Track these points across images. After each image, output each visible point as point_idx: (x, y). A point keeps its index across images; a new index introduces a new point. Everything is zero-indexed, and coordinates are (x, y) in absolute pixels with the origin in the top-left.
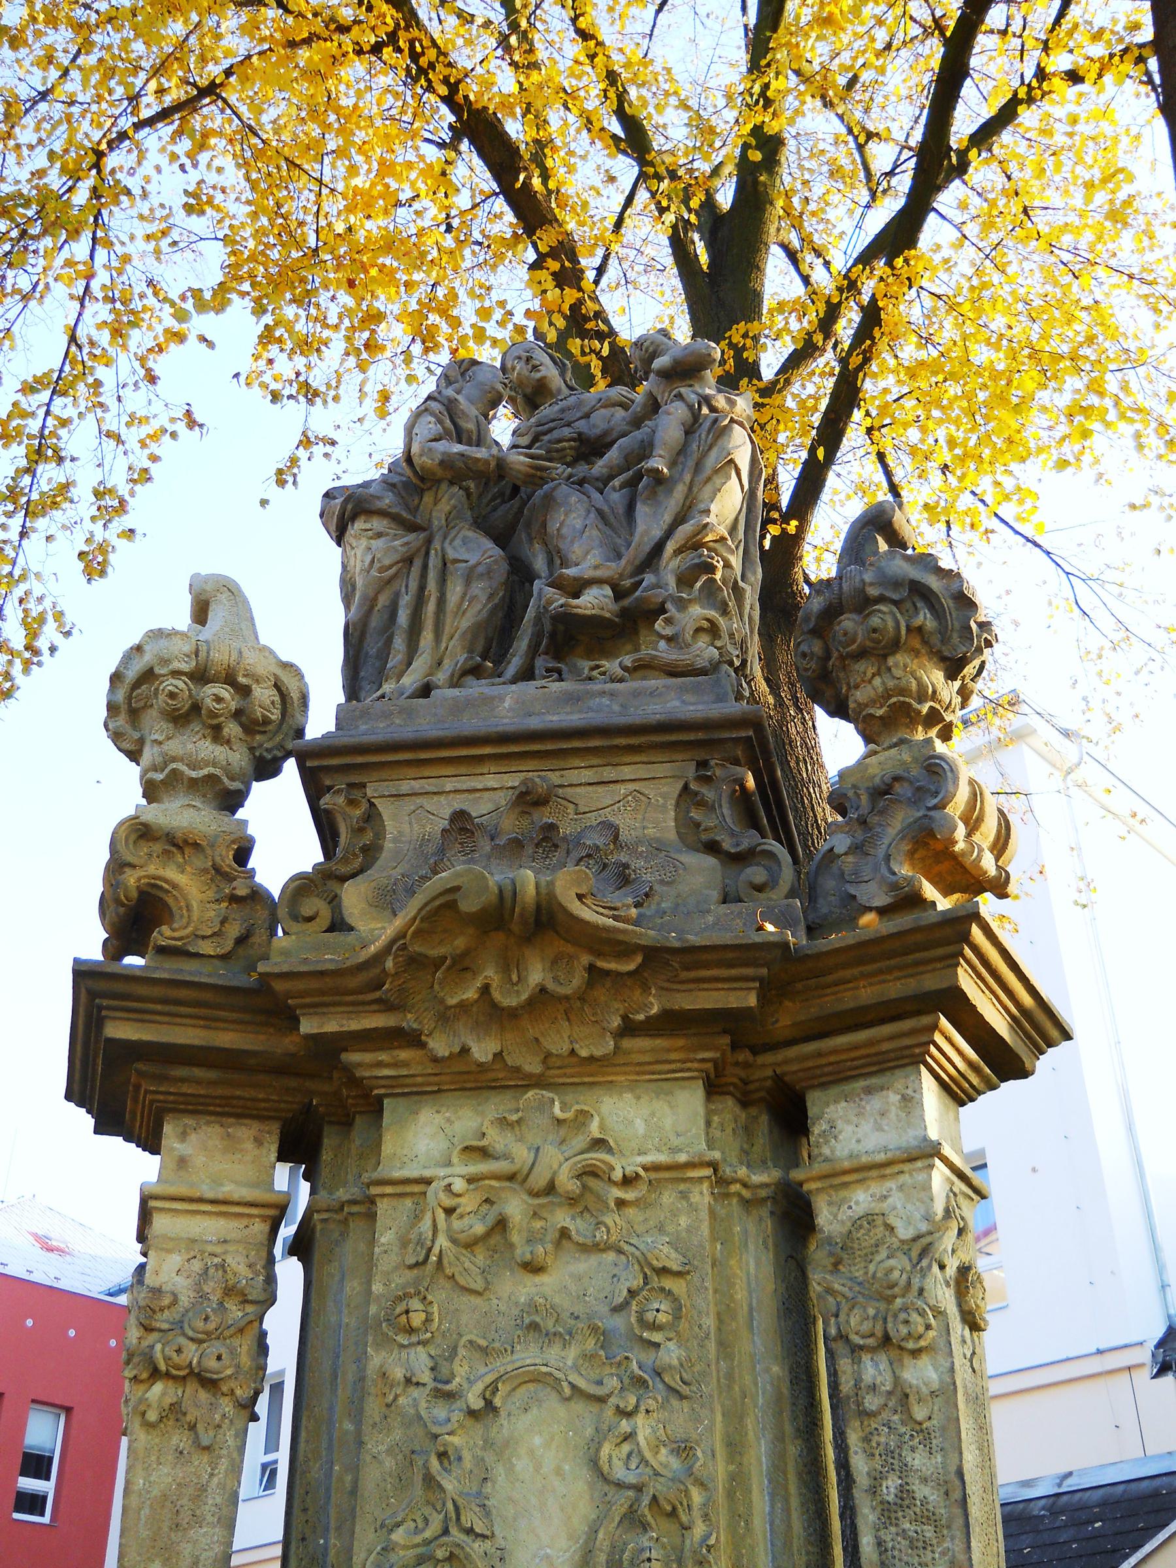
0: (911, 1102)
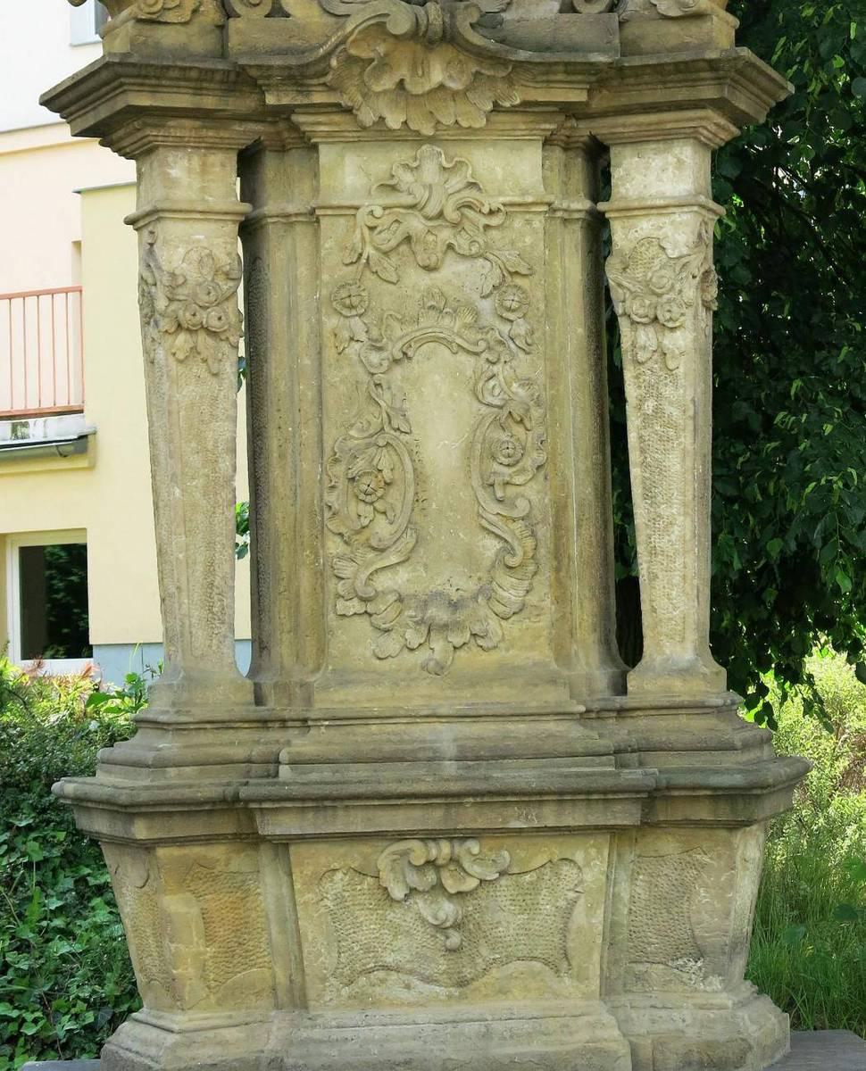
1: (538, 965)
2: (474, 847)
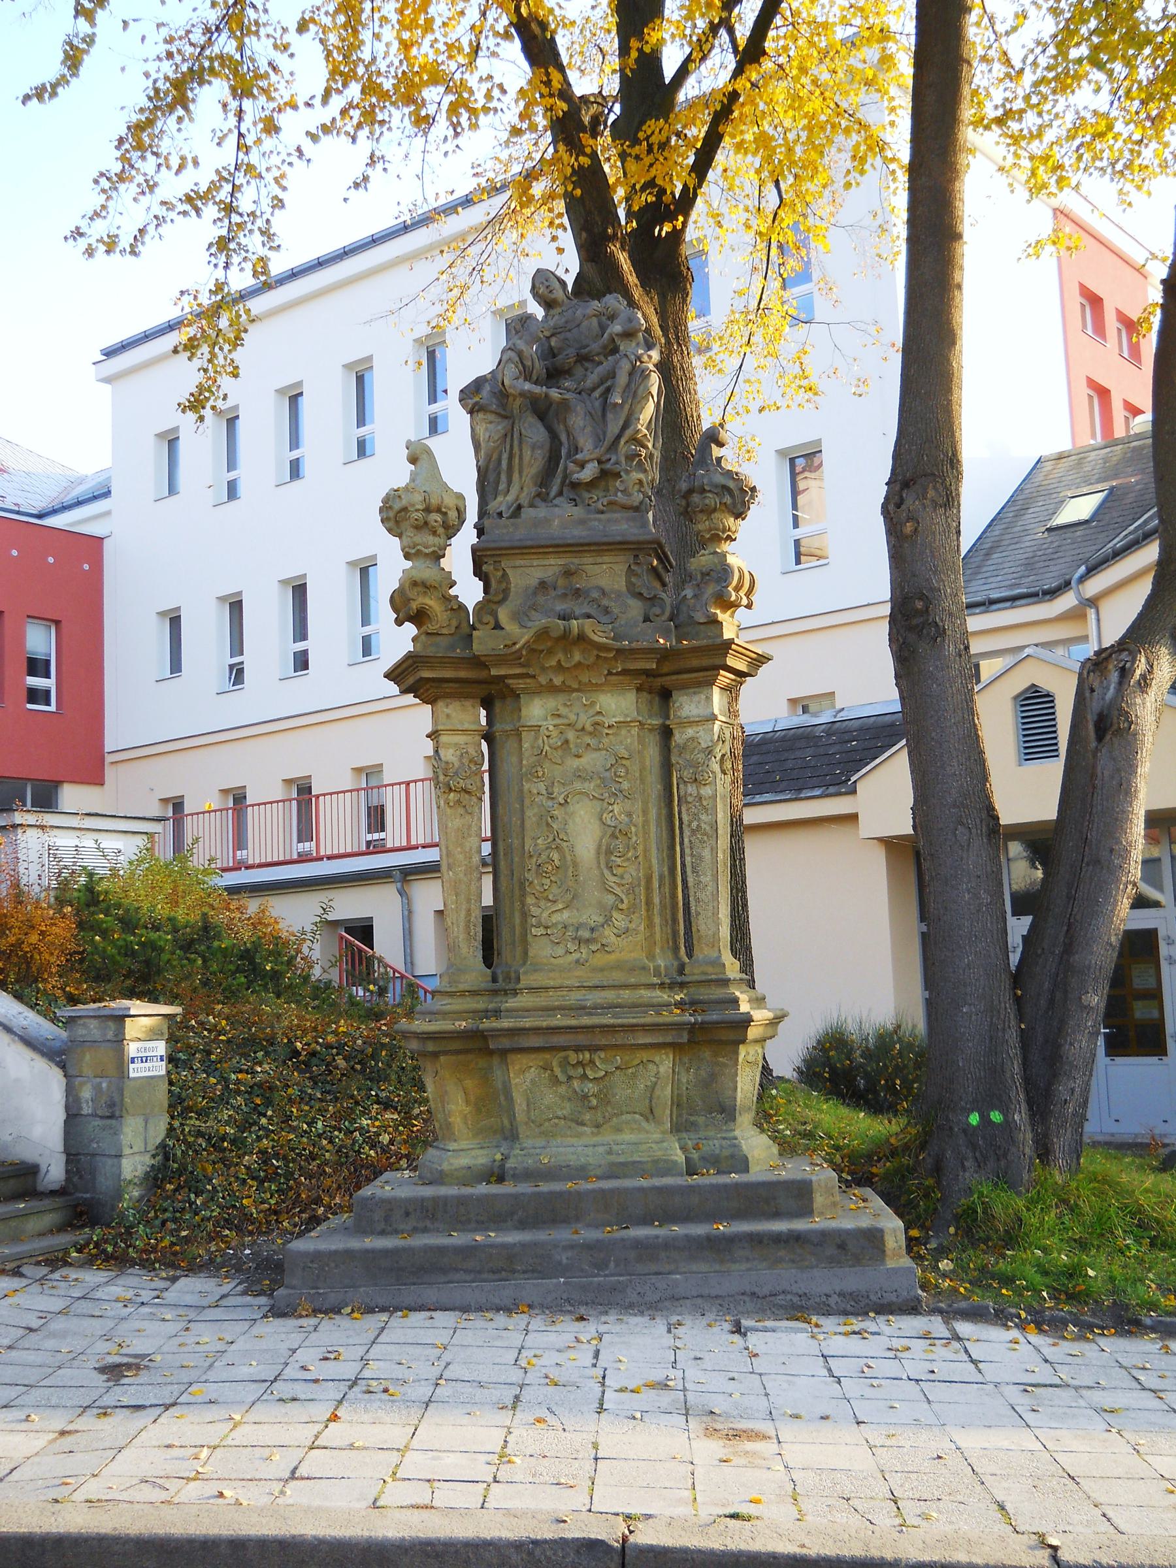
0: (709, 699)
1: (637, 1116)
2: (603, 1055)
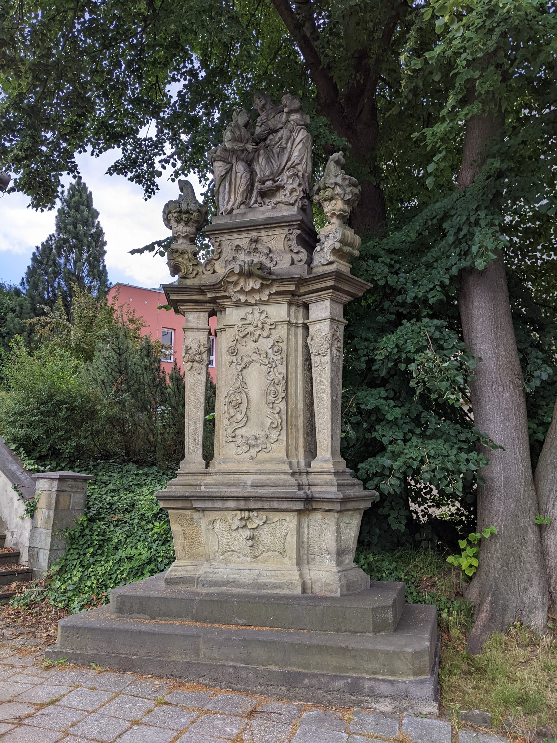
1: (277, 553)
2: (255, 514)
